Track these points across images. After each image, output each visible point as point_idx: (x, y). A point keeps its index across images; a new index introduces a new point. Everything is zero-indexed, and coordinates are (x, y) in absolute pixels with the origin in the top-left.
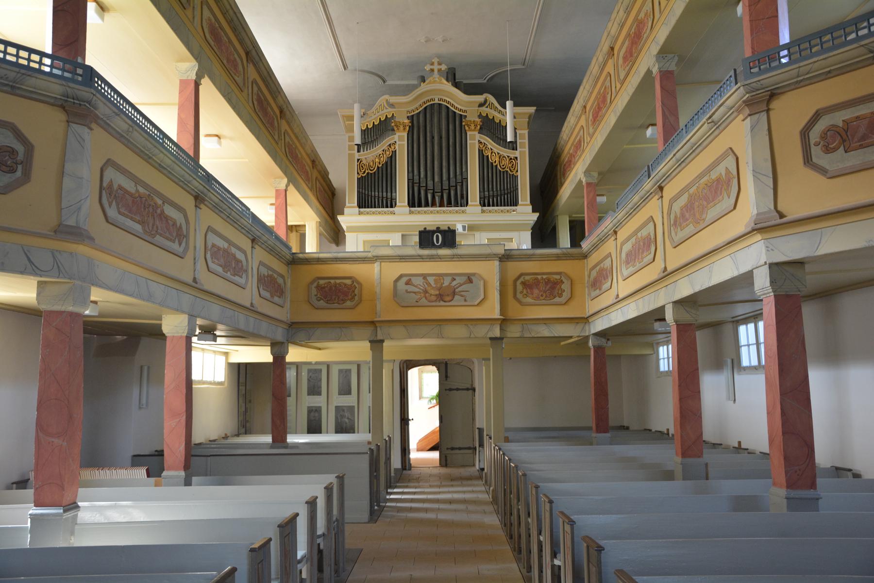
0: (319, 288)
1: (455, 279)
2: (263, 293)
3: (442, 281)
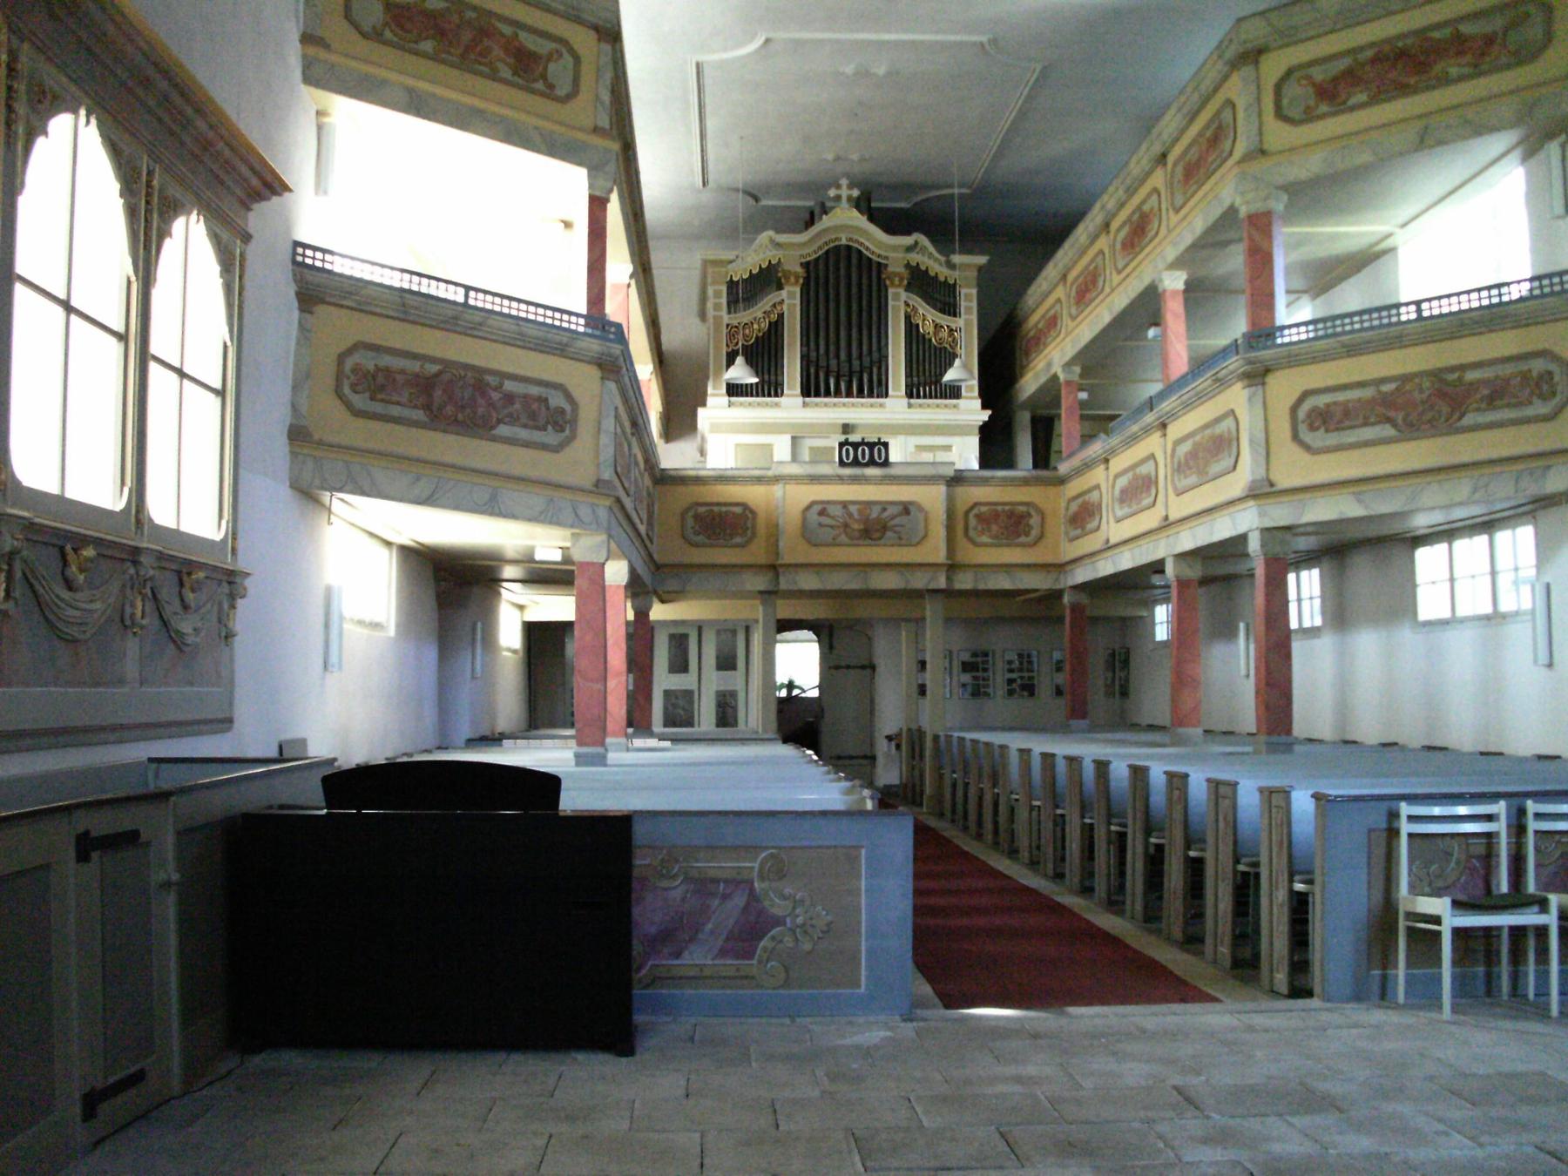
0: (696, 517)
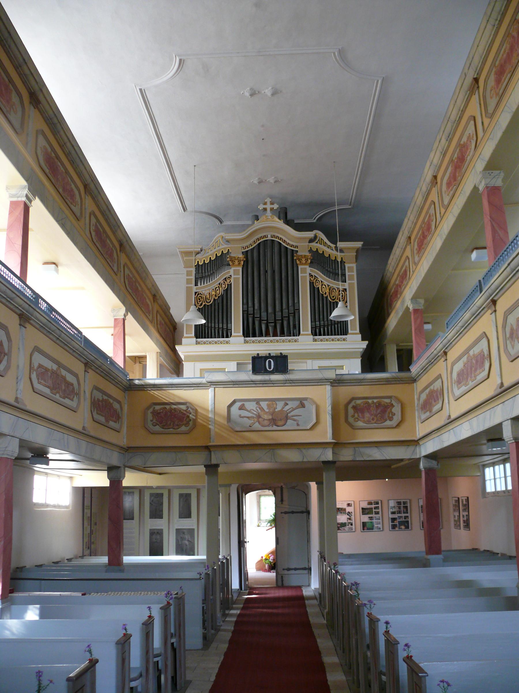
0: (155, 413)
1: (287, 404)
2: (96, 416)
3: (275, 406)
